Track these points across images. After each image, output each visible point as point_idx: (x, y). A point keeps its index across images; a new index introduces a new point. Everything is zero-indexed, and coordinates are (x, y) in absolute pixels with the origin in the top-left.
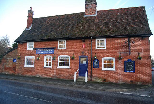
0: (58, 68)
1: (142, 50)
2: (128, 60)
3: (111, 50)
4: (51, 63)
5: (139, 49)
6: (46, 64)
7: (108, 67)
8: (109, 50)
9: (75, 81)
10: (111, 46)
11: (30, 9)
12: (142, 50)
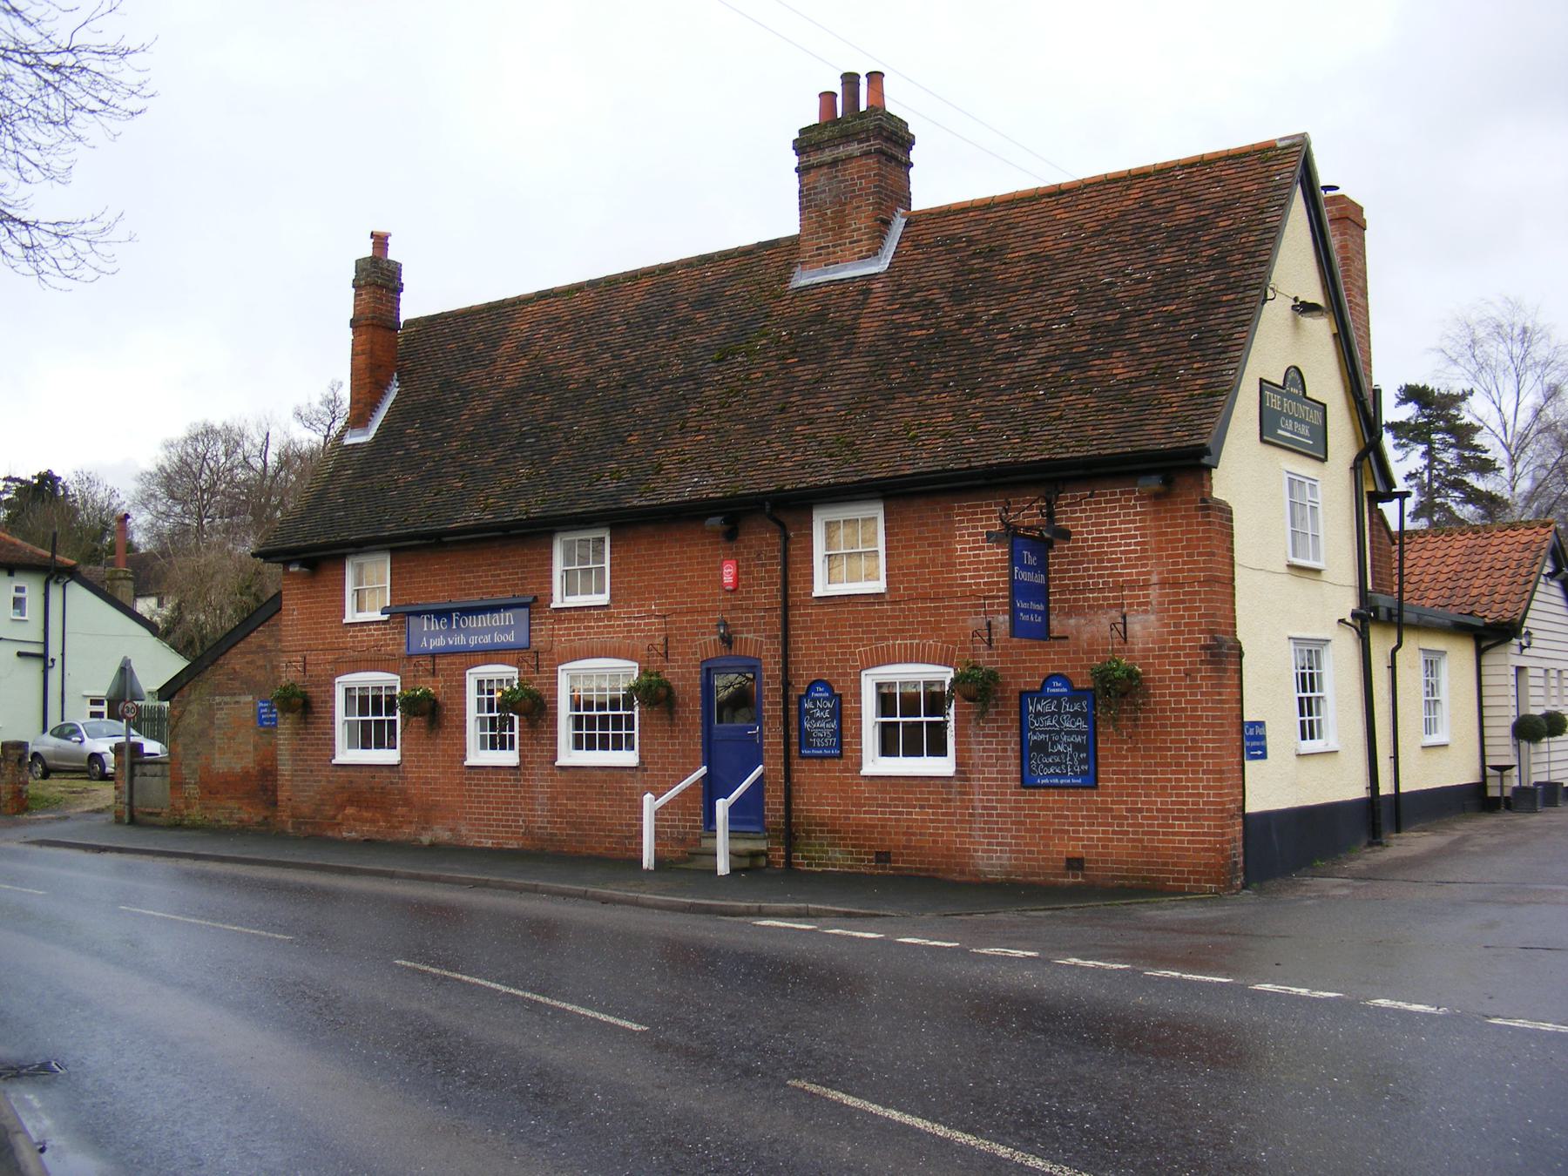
0: (562, 768)
1: (1154, 593)
2: (1049, 679)
3: (924, 599)
4: (630, 727)
5: (1132, 585)
6: (483, 738)
7: (913, 750)
8: (911, 599)
9: (648, 860)
10: (922, 565)
11: (367, 250)
12: (1154, 593)
